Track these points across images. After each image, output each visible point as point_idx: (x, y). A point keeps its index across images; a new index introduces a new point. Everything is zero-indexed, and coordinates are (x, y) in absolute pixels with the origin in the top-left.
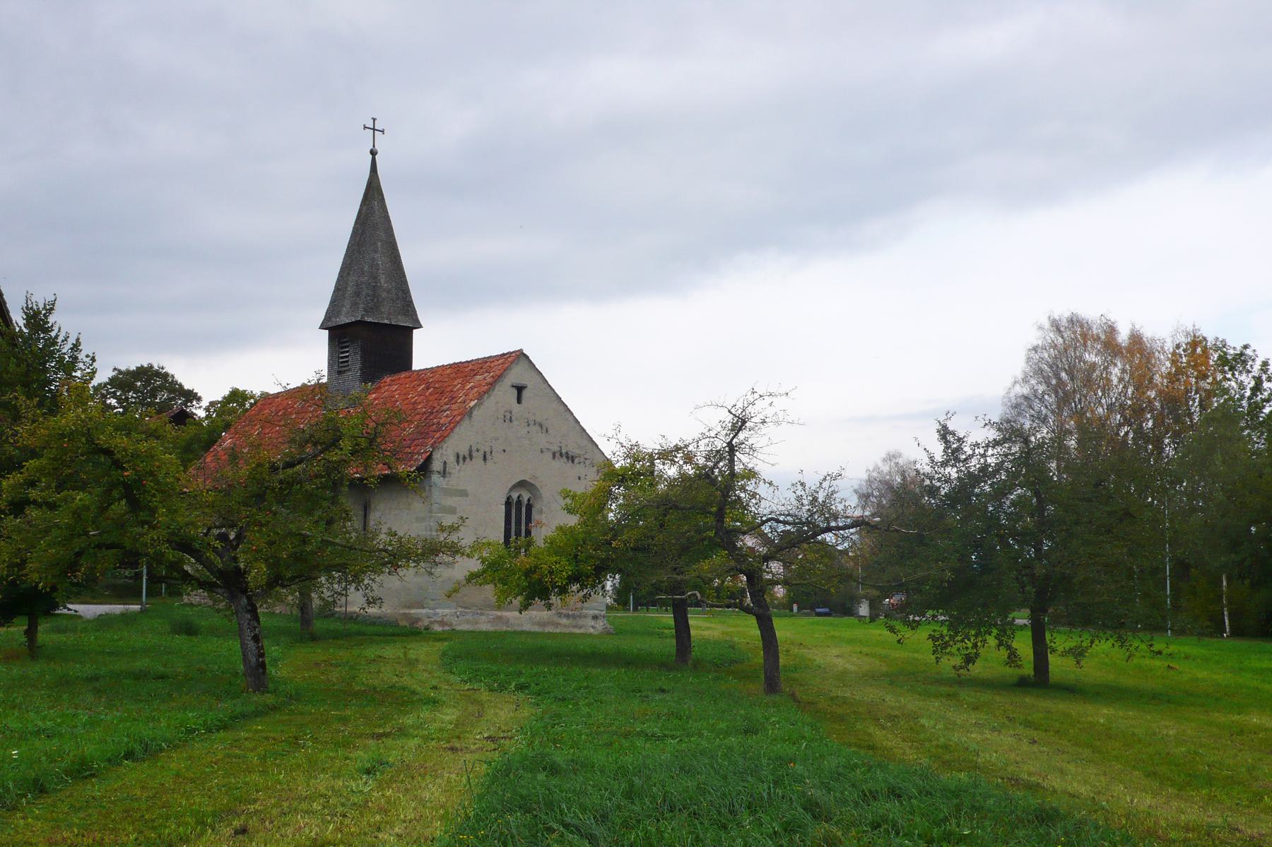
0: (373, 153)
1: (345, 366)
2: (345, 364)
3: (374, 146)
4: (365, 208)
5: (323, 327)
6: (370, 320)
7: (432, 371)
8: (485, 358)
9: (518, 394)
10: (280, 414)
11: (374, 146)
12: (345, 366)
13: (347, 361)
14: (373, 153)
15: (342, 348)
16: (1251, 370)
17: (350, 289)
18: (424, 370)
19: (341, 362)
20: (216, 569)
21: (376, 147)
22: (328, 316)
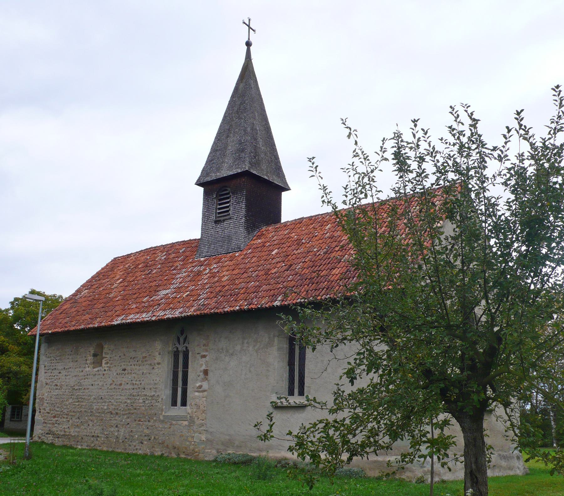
0: (248, 44)
1: (225, 216)
2: (226, 214)
3: (249, 39)
4: (241, 85)
5: (199, 183)
6: (254, 172)
7: (300, 221)
8: (123, 256)
9: (175, 359)
10: (140, 266)
11: (249, 39)
12: (225, 216)
13: (228, 211)
14: (248, 44)
15: (220, 200)
16: (471, 127)
17: (231, 148)
18: (150, 248)
19: (219, 213)
20: (302, 321)
21: (251, 40)
22: (205, 172)
